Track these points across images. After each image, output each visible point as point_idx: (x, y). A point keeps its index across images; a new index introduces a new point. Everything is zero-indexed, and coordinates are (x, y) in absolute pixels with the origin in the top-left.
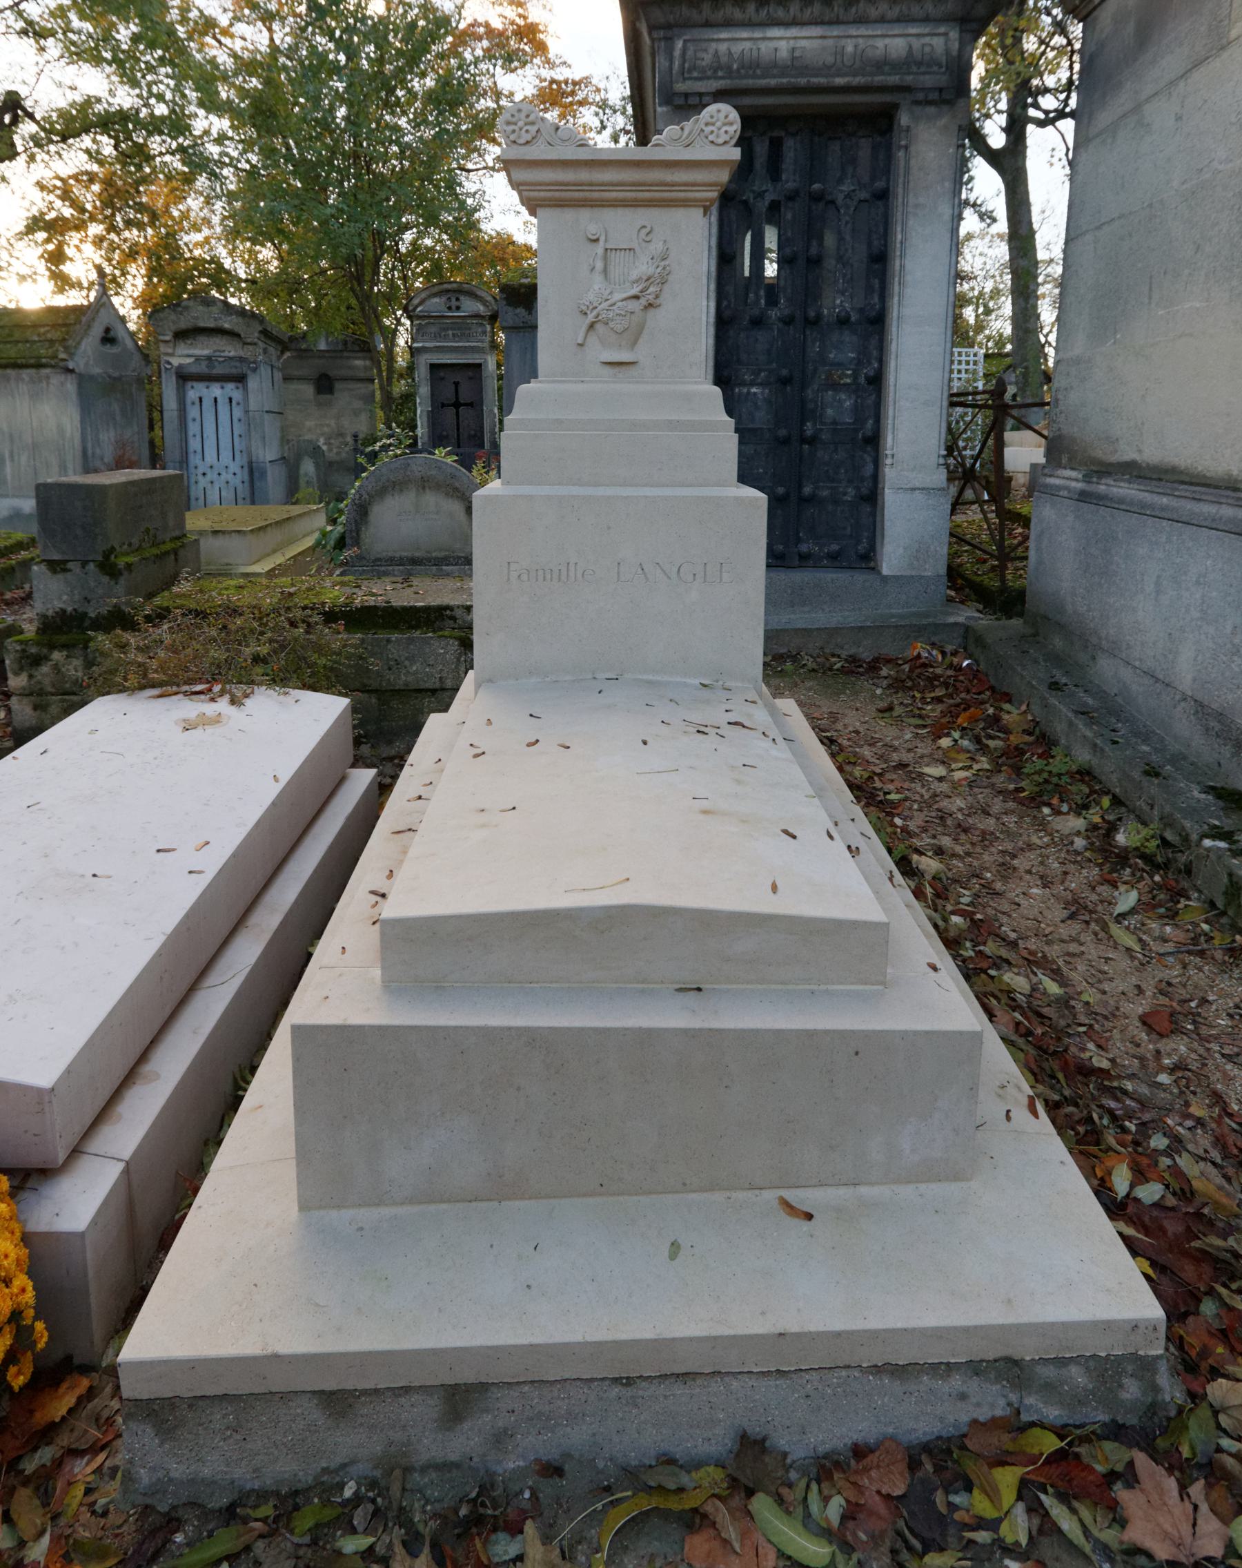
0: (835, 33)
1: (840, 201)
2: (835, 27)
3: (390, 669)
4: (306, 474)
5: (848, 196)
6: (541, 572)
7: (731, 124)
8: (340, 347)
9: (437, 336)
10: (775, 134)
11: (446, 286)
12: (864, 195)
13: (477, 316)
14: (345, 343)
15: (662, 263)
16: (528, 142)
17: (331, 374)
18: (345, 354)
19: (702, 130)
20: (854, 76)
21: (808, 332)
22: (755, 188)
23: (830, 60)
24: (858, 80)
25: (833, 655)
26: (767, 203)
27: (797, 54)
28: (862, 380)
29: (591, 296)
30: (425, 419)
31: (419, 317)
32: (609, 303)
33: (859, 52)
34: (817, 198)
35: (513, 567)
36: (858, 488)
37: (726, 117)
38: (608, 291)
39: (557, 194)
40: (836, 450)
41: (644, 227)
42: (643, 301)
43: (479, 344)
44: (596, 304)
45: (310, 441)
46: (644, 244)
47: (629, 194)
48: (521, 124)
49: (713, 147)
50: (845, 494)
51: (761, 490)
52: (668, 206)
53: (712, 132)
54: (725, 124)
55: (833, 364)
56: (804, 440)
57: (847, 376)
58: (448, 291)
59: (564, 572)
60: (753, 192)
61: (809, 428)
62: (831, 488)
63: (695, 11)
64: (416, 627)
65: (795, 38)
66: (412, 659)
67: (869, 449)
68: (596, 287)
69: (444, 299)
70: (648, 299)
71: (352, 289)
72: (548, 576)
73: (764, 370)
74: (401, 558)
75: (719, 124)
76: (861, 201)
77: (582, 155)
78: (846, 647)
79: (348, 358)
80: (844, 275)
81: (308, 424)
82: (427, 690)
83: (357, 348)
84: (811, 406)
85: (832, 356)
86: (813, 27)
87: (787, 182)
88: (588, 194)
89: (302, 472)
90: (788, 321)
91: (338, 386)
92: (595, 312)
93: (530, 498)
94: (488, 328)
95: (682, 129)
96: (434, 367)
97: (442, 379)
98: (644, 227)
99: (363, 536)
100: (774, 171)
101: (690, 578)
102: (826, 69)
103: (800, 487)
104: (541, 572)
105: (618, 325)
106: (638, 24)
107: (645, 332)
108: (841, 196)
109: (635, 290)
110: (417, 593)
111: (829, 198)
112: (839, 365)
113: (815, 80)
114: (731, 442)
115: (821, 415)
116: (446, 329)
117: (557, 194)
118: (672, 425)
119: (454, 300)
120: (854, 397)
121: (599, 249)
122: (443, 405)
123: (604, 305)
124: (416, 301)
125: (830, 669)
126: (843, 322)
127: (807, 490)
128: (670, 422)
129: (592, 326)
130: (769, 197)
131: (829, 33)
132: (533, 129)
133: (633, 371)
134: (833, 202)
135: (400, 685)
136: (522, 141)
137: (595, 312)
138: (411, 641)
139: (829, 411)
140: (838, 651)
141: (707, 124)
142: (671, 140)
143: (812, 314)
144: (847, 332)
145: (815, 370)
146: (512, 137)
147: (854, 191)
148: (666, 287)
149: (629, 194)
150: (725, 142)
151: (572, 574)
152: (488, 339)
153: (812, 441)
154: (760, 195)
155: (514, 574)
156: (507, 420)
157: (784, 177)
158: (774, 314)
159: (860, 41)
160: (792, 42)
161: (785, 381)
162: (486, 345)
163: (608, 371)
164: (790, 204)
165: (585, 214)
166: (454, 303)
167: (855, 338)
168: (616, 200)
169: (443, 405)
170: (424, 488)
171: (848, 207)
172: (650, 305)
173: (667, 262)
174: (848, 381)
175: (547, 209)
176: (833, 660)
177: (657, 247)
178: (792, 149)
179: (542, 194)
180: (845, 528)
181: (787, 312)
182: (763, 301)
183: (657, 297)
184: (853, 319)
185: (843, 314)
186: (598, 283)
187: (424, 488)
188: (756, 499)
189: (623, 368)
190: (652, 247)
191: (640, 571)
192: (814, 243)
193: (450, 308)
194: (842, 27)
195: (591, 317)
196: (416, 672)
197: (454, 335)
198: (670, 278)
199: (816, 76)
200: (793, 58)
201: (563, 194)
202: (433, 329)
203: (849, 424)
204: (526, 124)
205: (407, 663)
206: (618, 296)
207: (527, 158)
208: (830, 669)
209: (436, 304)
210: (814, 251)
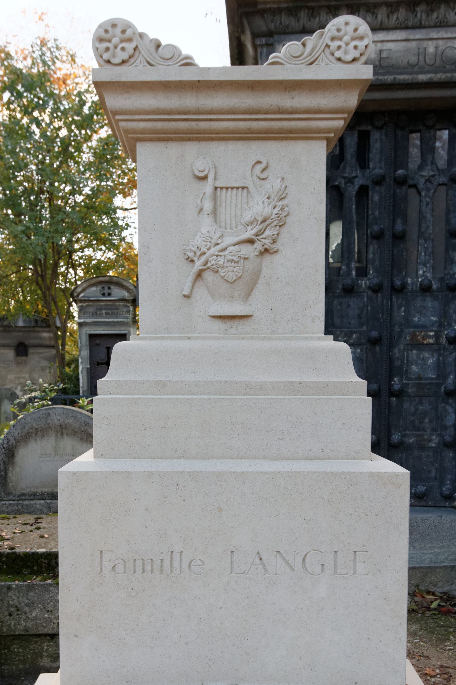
0: (418, 37)
1: (421, 186)
2: (417, 31)
3: (10, 615)
4: (5, 412)
5: (428, 180)
6: (139, 563)
7: (361, 38)
8: (33, 324)
9: (94, 314)
10: (363, 128)
11: (101, 279)
12: (443, 179)
13: (123, 300)
14: (36, 321)
15: (280, 203)
16: (124, 62)
17: (27, 342)
18: (37, 329)
19: (328, 46)
20: (436, 73)
21: (394, 299)
22: (346, 175)
23: (414, 59)
24: (440, 76)
25: (429, 593)
26: (357, 187)
27: (384, 55)
28: (443, 340)
29: (199, 241)
30: (85, 373)
31: (81, 301)
32: (218, 247)
33: (439, 52)
34: (401, 182)
35: (106, 556)
36: (441, 436)
37: (356, 30)
38: (218, 234)
39: (159, 125)
40: (421, 403)
41: (259, 162)
42: (258, 246)
43: (125, 320)
44: (203, 249)
45: (9, 389)
46: (259, 182)
47: (241, 124)
48: (115, 40)
49: (339, 65)
50: (430, 441)
51: (407, 468)
52: (286, 139)
53: (339, 48)
54: (353, 39)
55: (416, 326)
56: (392, 394)
57: (430, 337)
58: (101, 282)
59: (167, 563)
60: (344, 178)
61: (396, 383)
62: (418, 436)
63: (293, 19)
64: (37, 573)
65: (382, 41)
66: (31, 605)
67: (450, 401)
68: (204, 231)
69: (99, 288)
70: (263, 243)
71: (37, 284)
72: (148, 568)
73: (356, 332)
74: (43, 494)
75: (346, 38)
76: (440, 185)
77: (187, 75)
78: (440, 584)
79: (39, 331)
80: (426, 249)
81: (9, 377)
82: (46, 635)
83: (45, 325)
84: (397, 363)
85: (416, 319)
86: (398, 32)
87: (374, 169)
88: (194, 124)
89: (2, 411)
90: (376, 289)
91: (31, 351)
92: (203, 259)
93: (127, 474)
94: (131, 308)
95: (304, 45)
96: (91, 336)
97: (98, 345)
98: (259, 162)
99: (10, 475)
100: (363, 160)
101: (318, 569)
102: (410, 68)
103: (389, 434)
104: (139, 563)
105: (230, 272)
106: (242, 38)
107: (260, 281)
108: (422, 180)
109: (249, 234)
110: (43, 537)
111: (411, 182)
112: (423, 327)
113: (401, 77)
114: (364, 407)
115: (407, 371)
116: (101, 310)
117: (159, 125)
118: (293, 388)
119: (106, 288)
120: (436, 356)
121: (208, 187)
122: (98, 364)
123: (214, 250)
124: (79, 290)
125: (429, 609)
126: (426, 289)
127: (396, 438)
128: (292, 383)
129: (199, 275)
130: (358, 182)
131: (412, 37)
132: (130, 47)
133: (246, 326)
134: (415, 186)
135: (20, 630)
136: (117, 60)
137: (203, 259)
138: (31, 587)
139: (414, 368)
140: (432, 589)
141: (333, 39)
142: (290, 59)
143: (398, 283)
144: (429, 299)
145: (401, 332)
146: (106, 56)
147: (433, 176)
148: (284, 229)
149: (241, 124)
150: (354, 60)
151: (176, 564)
152: (131, 316)
153: (400, 394)
154: (350, 181)
155: (107, 566)
156: (101, 383)
157: (371, 165)
158: (364, 283)
159: (441, 42)
160: (379, 45)
161: (374, 342)
162: (130, 320)
163: (218, 324)
164: (377, 188)
165: (191, 149)
166: (106, 291)
167: (436, 304)
168: (226, 131)
169: (98, 364)
170: (62, 434)
171: (428, 190)
172: (266, 250)
173: (285, 202)
174: (431, 341)
175: (148, 144)
176: (429, 597)
177: (274, 184)
178: (377, 141)
179: (142, 125)
180: (429, 472)
181: (376, 281)
182: (354, 273)
183: (274, 242)
184: (434, 287)
185: (426, 282)
186: (206, 225)
187: (62, 434)
188: (397, 475)
189: (236, 323)
190: (267, 185)
191: (257, 561)
192: (399, 221)
193: (103, 295)
194: (424, 31)
195: (198, 265)
196: (36, 618)
197: (106, 314)
198: (289, 220)
199: (402, 74)
200: (381, 59)
201: (166, 125)
202: (91, 310)
203: (432, 379)
204: (122, 41)
205: (27, 609)
206: (228, 240)
207: (123, 79)
208: (429, 609)
209: (94, 292)
210: (399, 227)
